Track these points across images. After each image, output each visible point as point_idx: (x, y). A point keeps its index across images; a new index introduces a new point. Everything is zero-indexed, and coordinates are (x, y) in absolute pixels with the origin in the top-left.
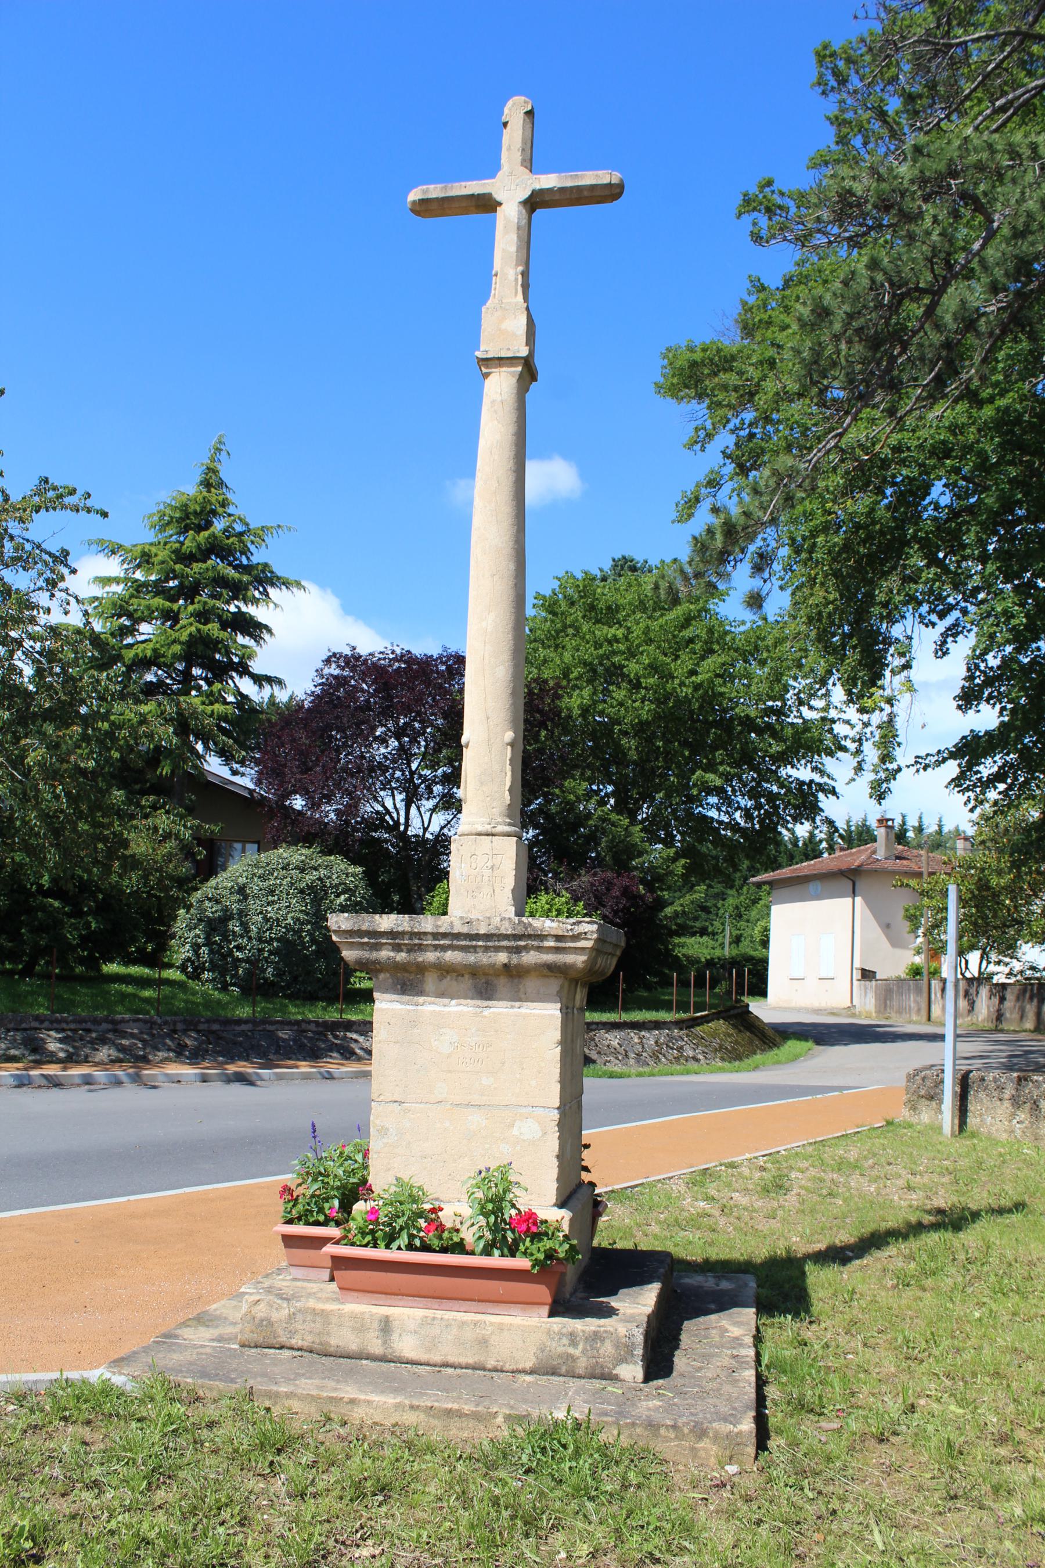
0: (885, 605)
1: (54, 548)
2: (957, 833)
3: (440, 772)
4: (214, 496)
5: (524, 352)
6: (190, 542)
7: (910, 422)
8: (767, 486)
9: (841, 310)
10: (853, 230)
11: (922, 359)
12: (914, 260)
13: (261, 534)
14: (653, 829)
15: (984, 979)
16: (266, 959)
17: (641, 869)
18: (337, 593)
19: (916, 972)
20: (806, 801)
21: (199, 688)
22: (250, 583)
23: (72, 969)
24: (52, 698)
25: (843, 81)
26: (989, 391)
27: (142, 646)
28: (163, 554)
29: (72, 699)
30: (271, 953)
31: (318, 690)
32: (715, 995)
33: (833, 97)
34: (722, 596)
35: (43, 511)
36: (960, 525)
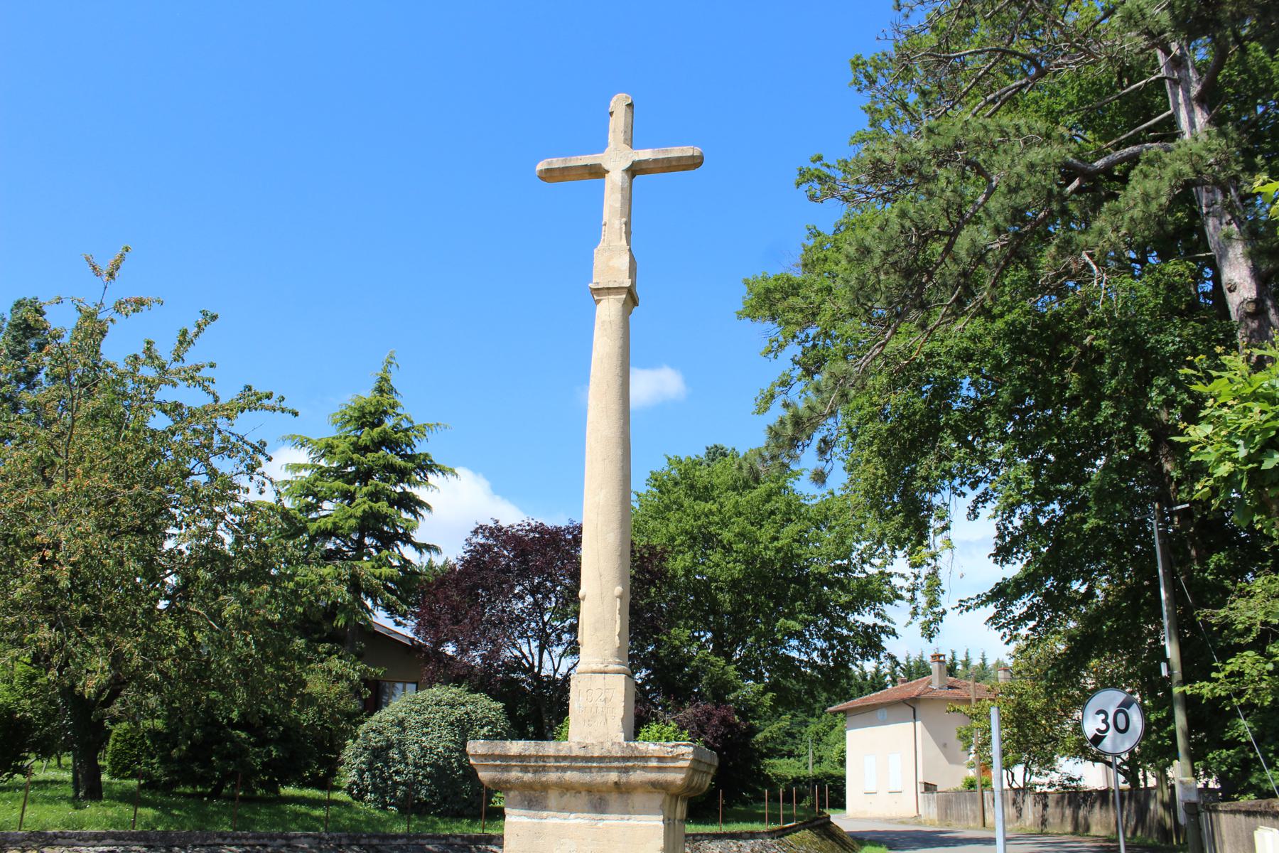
0: (925, 479)
1: (253, 439)
2: (999, 665)
3: (567, 623)
4: (386, 400)
5: (627, 283)
6: (366, 436)
7: (939, 333)
8: (826, 386)
9: (879, 249)
10: (885, 188)
11: (945, 285)
12: (933, 210)
13: (423, 430)
14: (746, 667)
15: (1027, 789)
16: (420, 782)
17: (736, 700)
18: (488, 476)
19: (971, 785)
20: (871, 642)
21: (370, 555)
22: (413, 470)
23: (254, 792)
24: (246, 561)
25: (873, 82)
26: (1000, 308)
27: (324, 520)
28: (343, 446)
29: (264, 562)
30: (425, 777)
31: (467, 556)
32: (803, 808)
33: (866, 93)
34: (796, 475)
35: (246, 411)
36: (983, 414)
